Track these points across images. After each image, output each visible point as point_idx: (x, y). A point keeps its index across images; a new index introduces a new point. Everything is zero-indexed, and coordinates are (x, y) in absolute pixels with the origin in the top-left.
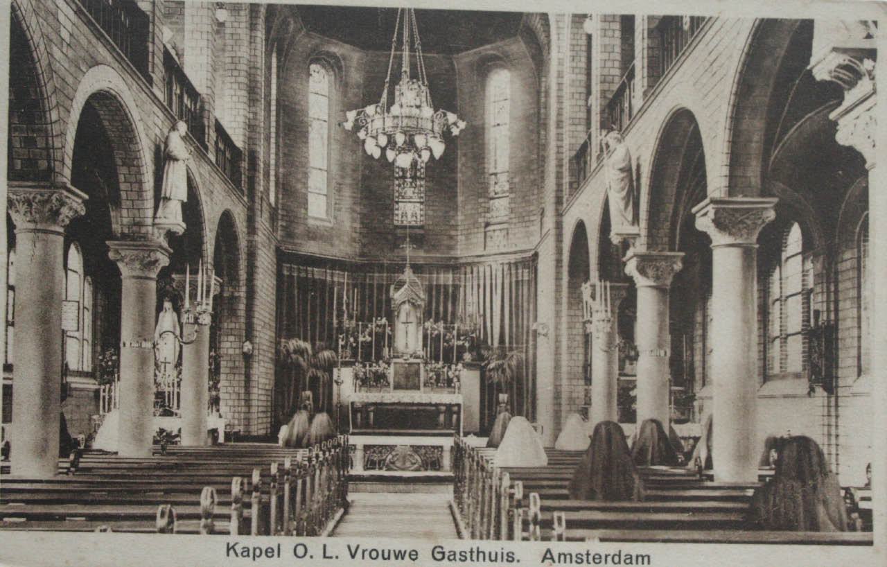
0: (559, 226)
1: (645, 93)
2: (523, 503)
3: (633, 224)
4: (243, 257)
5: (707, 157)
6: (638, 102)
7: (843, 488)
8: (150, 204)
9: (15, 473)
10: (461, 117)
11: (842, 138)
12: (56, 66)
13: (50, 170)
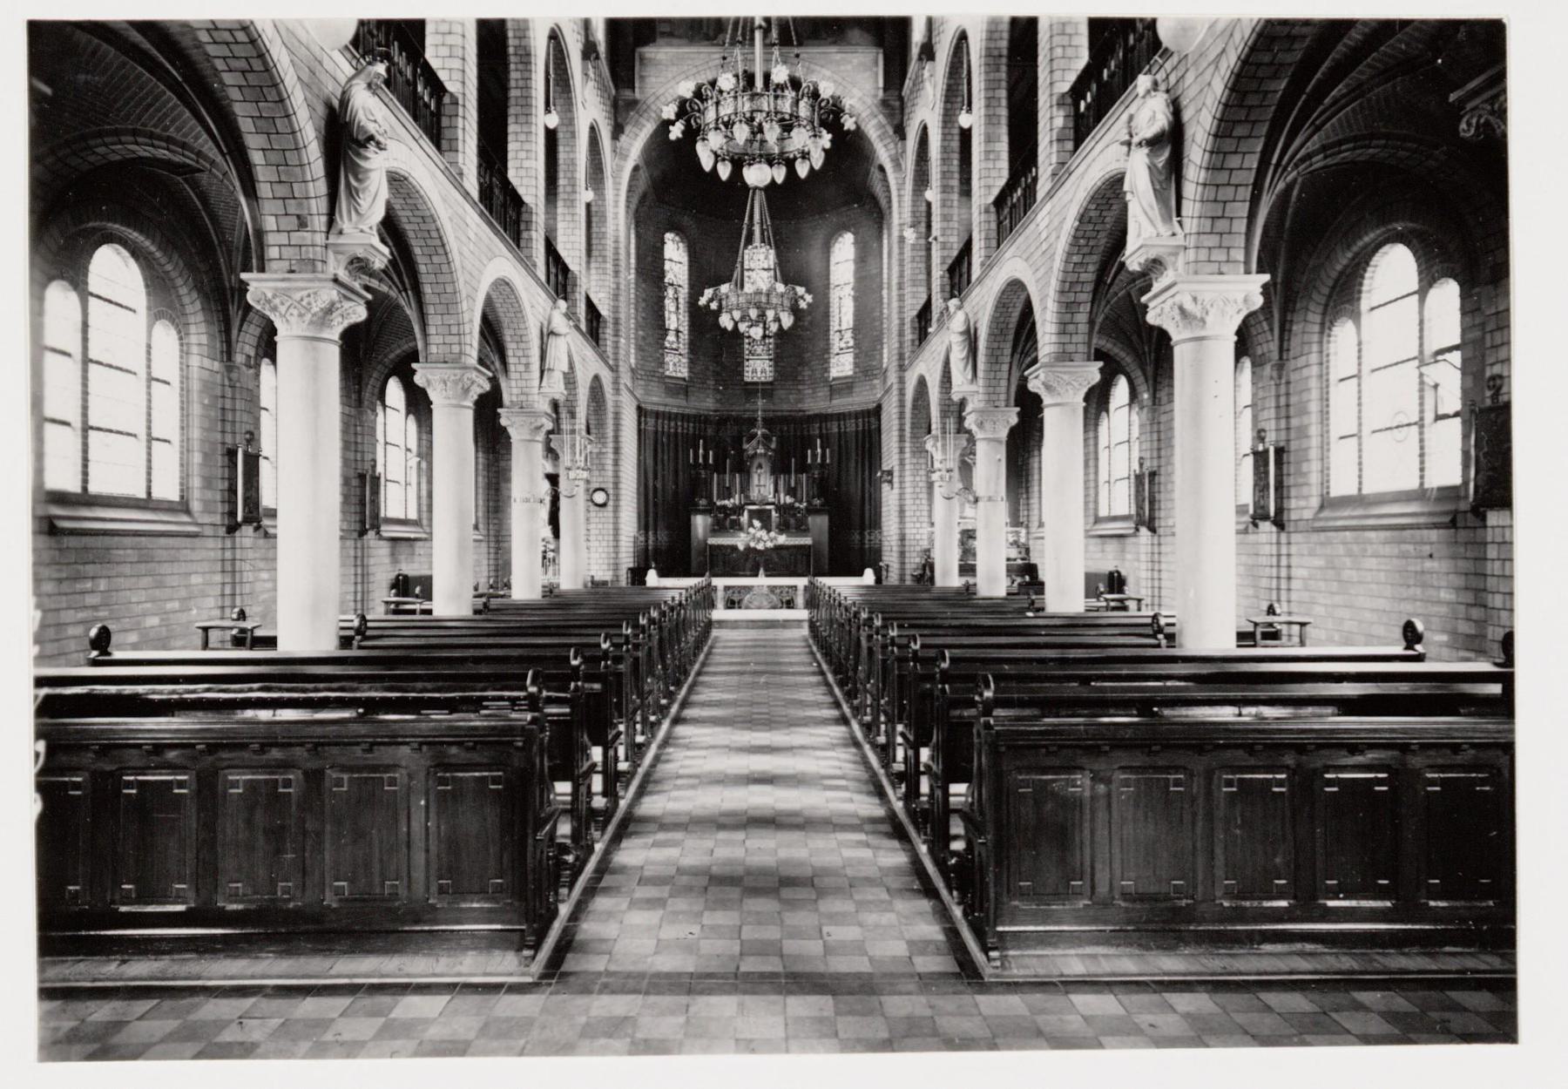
0: (902, 381)
1: (982, 264)
2: (703, 454)
4: (610, 416)
5: (1038, 326)
7: (638, 575)
8: (537, 374)
9: (437, 613)
10: (808, 291)
11: (1152, 318)
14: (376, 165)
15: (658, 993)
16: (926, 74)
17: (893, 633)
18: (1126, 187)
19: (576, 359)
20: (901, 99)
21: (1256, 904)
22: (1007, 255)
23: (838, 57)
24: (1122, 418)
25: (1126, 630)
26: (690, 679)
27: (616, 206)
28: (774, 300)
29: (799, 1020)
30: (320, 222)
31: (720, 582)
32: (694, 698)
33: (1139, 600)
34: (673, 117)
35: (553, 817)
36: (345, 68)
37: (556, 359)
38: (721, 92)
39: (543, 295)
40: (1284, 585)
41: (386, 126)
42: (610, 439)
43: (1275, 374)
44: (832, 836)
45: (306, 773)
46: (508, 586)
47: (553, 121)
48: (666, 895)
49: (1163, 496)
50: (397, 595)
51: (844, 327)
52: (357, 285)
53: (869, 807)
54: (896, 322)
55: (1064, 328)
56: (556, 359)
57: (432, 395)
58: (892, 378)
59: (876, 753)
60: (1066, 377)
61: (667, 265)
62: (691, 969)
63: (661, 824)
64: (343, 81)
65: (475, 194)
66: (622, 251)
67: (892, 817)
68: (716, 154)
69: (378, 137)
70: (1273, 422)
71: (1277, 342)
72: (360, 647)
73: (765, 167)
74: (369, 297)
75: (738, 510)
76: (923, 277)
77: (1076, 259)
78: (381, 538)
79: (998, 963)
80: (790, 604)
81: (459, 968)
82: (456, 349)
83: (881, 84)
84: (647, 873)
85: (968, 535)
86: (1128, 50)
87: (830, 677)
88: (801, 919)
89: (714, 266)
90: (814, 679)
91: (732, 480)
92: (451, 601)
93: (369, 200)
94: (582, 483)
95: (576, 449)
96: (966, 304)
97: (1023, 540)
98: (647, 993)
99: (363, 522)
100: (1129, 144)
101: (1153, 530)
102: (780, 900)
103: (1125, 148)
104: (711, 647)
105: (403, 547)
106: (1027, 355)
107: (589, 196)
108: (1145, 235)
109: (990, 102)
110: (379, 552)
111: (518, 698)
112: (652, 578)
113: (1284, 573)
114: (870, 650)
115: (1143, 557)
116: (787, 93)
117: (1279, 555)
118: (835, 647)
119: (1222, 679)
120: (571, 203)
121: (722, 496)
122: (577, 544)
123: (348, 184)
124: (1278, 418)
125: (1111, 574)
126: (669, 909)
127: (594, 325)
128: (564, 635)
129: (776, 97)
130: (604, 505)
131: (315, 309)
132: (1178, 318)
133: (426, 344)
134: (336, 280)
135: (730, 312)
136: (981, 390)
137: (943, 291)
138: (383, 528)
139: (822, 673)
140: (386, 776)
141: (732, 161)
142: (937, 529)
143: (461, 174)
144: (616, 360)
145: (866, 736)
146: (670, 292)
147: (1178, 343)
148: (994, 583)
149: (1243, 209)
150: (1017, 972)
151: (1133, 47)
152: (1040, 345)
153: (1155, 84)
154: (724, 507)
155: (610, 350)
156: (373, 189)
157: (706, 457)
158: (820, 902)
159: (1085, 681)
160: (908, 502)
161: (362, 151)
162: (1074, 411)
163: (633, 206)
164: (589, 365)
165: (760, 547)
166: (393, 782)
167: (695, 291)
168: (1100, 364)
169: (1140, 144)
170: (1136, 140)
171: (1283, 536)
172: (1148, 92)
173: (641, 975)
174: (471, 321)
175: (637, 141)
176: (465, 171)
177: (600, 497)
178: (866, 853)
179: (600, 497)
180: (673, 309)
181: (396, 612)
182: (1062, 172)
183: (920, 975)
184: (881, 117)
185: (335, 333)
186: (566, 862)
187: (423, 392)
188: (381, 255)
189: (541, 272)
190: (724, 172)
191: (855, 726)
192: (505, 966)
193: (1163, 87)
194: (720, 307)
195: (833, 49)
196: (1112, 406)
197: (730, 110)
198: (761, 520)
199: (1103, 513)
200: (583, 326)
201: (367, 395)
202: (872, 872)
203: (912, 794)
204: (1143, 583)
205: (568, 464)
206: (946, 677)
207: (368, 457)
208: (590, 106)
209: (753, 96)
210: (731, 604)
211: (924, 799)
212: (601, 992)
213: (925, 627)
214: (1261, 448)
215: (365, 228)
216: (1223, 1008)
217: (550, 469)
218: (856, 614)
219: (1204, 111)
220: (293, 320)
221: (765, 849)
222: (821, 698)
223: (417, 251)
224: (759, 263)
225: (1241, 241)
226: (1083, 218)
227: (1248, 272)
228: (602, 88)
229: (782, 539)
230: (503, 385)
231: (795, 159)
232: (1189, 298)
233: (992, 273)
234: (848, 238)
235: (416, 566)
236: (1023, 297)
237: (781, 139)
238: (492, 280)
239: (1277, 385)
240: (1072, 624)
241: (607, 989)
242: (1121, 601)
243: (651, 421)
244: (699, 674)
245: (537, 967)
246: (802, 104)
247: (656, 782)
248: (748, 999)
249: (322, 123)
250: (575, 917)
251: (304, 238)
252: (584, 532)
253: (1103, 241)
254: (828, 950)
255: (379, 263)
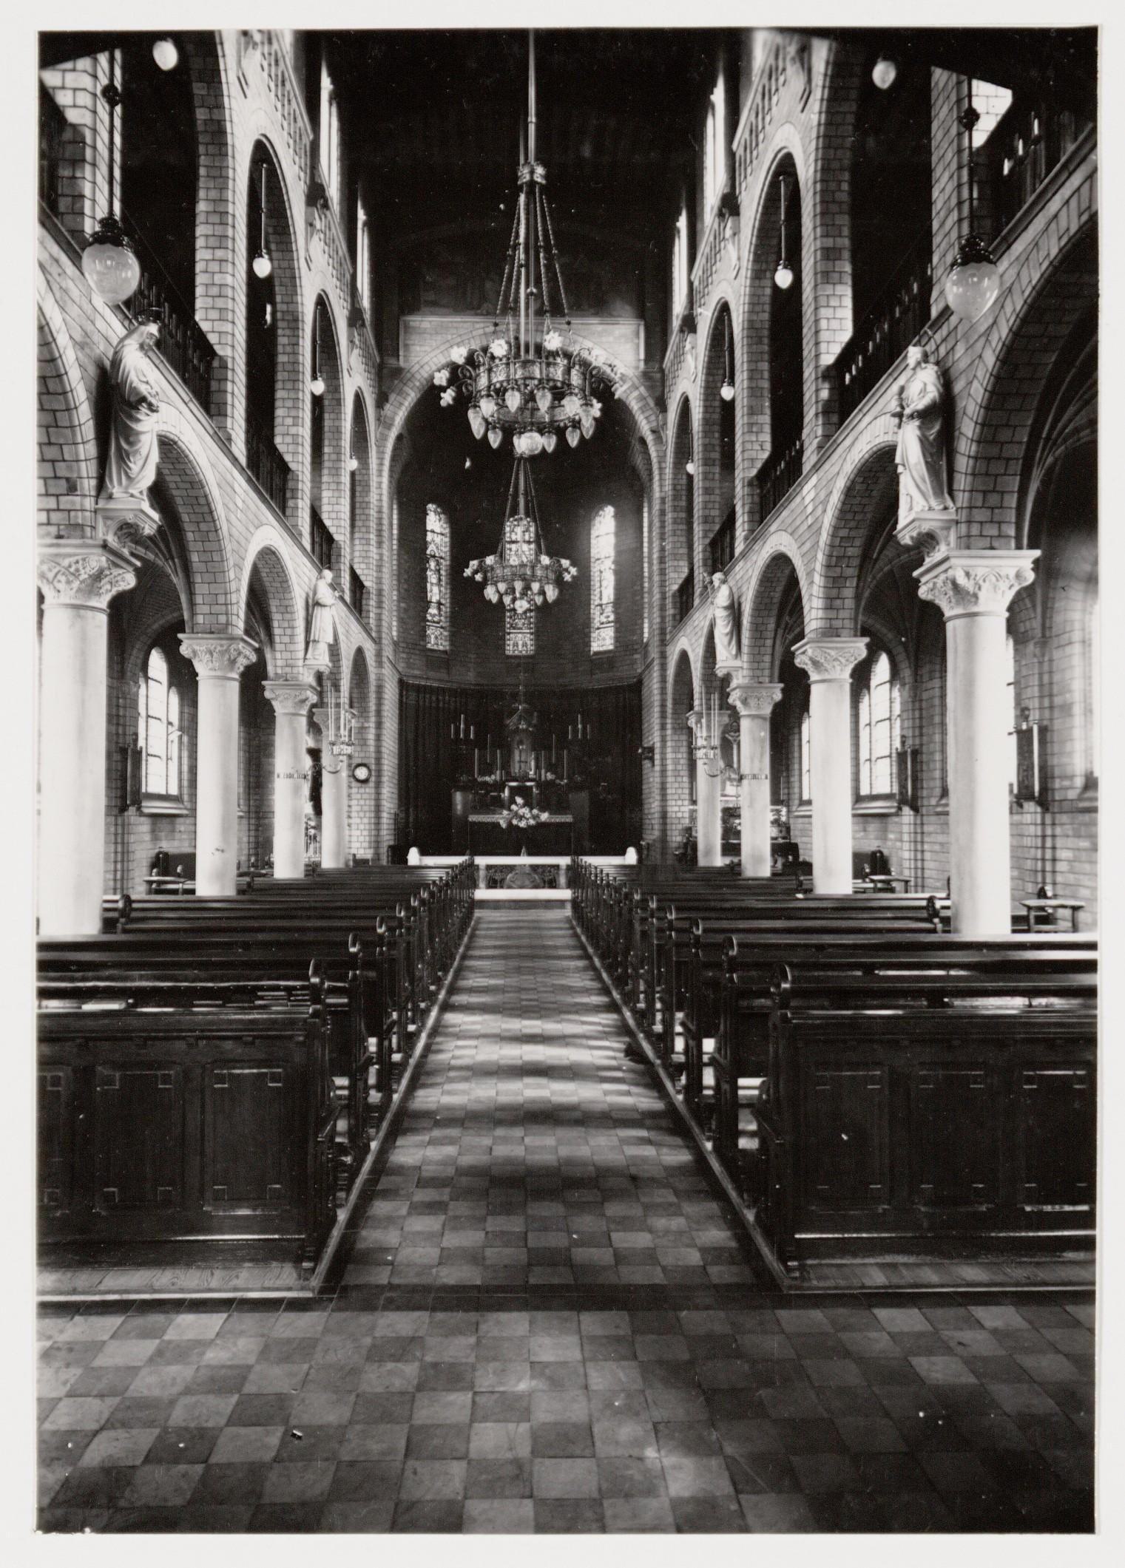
0: (663, 656)
1: (746, 538)
3: (736, 656)
4: (372, 688)
5: (805, 601)
6: (739, 547)
7: (398, 854)
8: (302, 646)
10: (573, 564)
11: (923, 592)
12: (234, 531)
13: (228, 624)
14: (148, 427)
15: (445, 1310)
16: (688, 346)
17: (672, 916)
18: (898, 460)
19: (340, 630)
20: (662, 371)
21: (1057, 1208)
22: (773, 528)
23: (600, 328)
24: (884, 697)
25: (899, 914)
26: (456, 963)
27: (380, 475)
28: (539, 573)
29: (593, 1339)
30: (89, 485)
31: (482, 861)
32: (463, 983)
33: (907, 882)
34: (444, 383)
35: (332, 1116)
36: (116, 327)
37: (322, 629)
38: (493, 358)
39: (309, 564)
40: (1048, 867)
41: (157, 388)
42: (372, 714)
43: (1038, 651)
44: (613, 1132)
45: (75, 1071)
46: (271, 865)
47: (319, 387)
48: (446, 1198)
49: (925, 775)
50: (158, 874)
51: (604, 601)
52: (126, 552)
53: (644, 1100)
54: (657, 596)
55: (831, 602)
56: (322, 629)
57: (199, 667)
58: (654, 653)
59: (652, 1043)
60: (833, 653)
61: (429, 537)
62: (478, 1283)
63: (433, 1119)
64: (115, 342)
65: (243, 460)
66: (385, 522)
67: (671, 1109)
68: (486, 420)
69: (150, 399)
70: (1036, 701)
71: (1039, 617)
72: (125, 931)
73: (536, 435)
74: (138, 564)
75: (500, 786)
76: (684, 551)
77: (843, 533)
78: (142, 814)
79: (797, 1274)
80: (552, 884)
81: (235, 1282)
82: (222, 619)
83: (642, 356)
84: (424, 1174)
85: (731, 814)
86: (894, 323)
87: (597, 962)
88: (586, 1223)
89: (476, 538)
90: (581, 963)
91: (494, 755)
92: (213, 880)
93: (140, 463)
94: (344, 758)
95: (341, 721)
96: (730, 579)
97: (784, 819)
98: (434, 1309)
99: (124, 797)
100: (900, 415)
101: (916, 809)
102: (565, 1203)
103: (896, 420)
104: (475, 929)
105: (164, 824)
106: (791, 630)
107: (353, 464)
108: (917, 508)
109: (753, 374)
110: (142, 828)
111: (294, 988)
112: (414, 857)
113: (1048, 855)
114: (644, 934)
115: (906, 837)
116: (559, 360)
117: (1044, 837)
118: (603, 930)
119: (1000, 967)
120: (336, 472)
121: (482, 773)
122: (331, 824)
123: (119, 448)
124: (1041, 697)
125: (874, 854)
126: (450, 1213)
127: (357, 596)
128: (330, 918)
129: (548, 365)
130: (365, 781)
131: (83, 576)
132: (951, 593)
133: (193, 614)
134: (105, 546)
135: (495, 584)
136: (745, 665)
137: (705, 565)
138: (144, 804)
139: (589, 957)
140: (159, 1073)
141: (504, 430)
142: (701, 807)
143: (229, 439)
144: (379, 632)
145: (639, 1024)
146: (432, 564)
147: (951, 618)
148: (758, 860)
149: (1015, 483)
150: (815, 1284)
151: (900, 319)
152: (806, 620)
153: (926, 357)
154: (485, 783)
155: (372, 622)
156: (144, 452)
157: (467, 731)
158: (606, 1204)
159: (869, 969)
160: (670, 779)
161: (133, 412)
162: (841, 687)
163: (396, 476)
164: (353, 638)
165: (523, 824)
166: (166, 1079)
167: (458, 562)
168: (867, 640)
169: (912, 416)
170: (907, 411)
171: (1048, 818)
172: (918, 364)
173: (426, 1289)
174: (238, 590)
175: (400, 412)
176: (234, 436)
177: (362, 773)
178: (649, 1151)
179: (362, 773)
180: (434, 581)
181: (158, 892)
182: (827, 444)
183: (715, 1286)
184: (642, 389)
185: (103, 602)
186: (344, 1164)
187: (188, 664)
188: (151, 520)
189: (307, 542)
190: (495, 440)
191: (628, 1014)
192: (280, 1281)
193: (932, 359)
194: (485, 580)
195: (594, 320)
196: (873, 683)
197: (502, 377)
198: (523, 797)
199: (864, 791)
200: (347, 598)
201: (129, 667)
202: (657, 1172)
203: (695, 1085)
204: (906, 864)
205: (332, 738)
206: (734, 965)
207: (130, 731)
208: (355, 377)
209: (526, 364)
210: (493, 884)
211: (709, 1092)
212: (385, 1308)
213: (707, 909)
214: (1024, 727)
215: (135, 492)
216: (1030, 1322)
217: (311, 744)
218: (628, 896)
219: (976, 384)
220: (61, 586)
221: (544, 1147)
222: (589, 984)
223: (185, 518)
224: (520, 539)
225: (1012, 516)
226: (849, 492)
227: (1019, 547)
228: (367, 356)
229: (545, 817)
230: (268, 656)
231: (566, 427)
232: (962, 574)
233: (756, 547)
234: (609, 511)
235: (176, 843)
236: (787, 572)
237: (552, 408)
238: (259, 548)
239: (1041, 663)
240: (843, 907)
241: (391, 1305)
242: (888, 882)
243: (413, 695)
244: (464, 957)
245: (316, 1282)
246: (574, 372)
247: (429, 1074)
248: (540, 1315)
249: (94, 384)
250: (353, 1223)
251: (73, 503)
252: (346, 808)
253: (869, 516)
254: (620, 1258)
255: (149, 529)
